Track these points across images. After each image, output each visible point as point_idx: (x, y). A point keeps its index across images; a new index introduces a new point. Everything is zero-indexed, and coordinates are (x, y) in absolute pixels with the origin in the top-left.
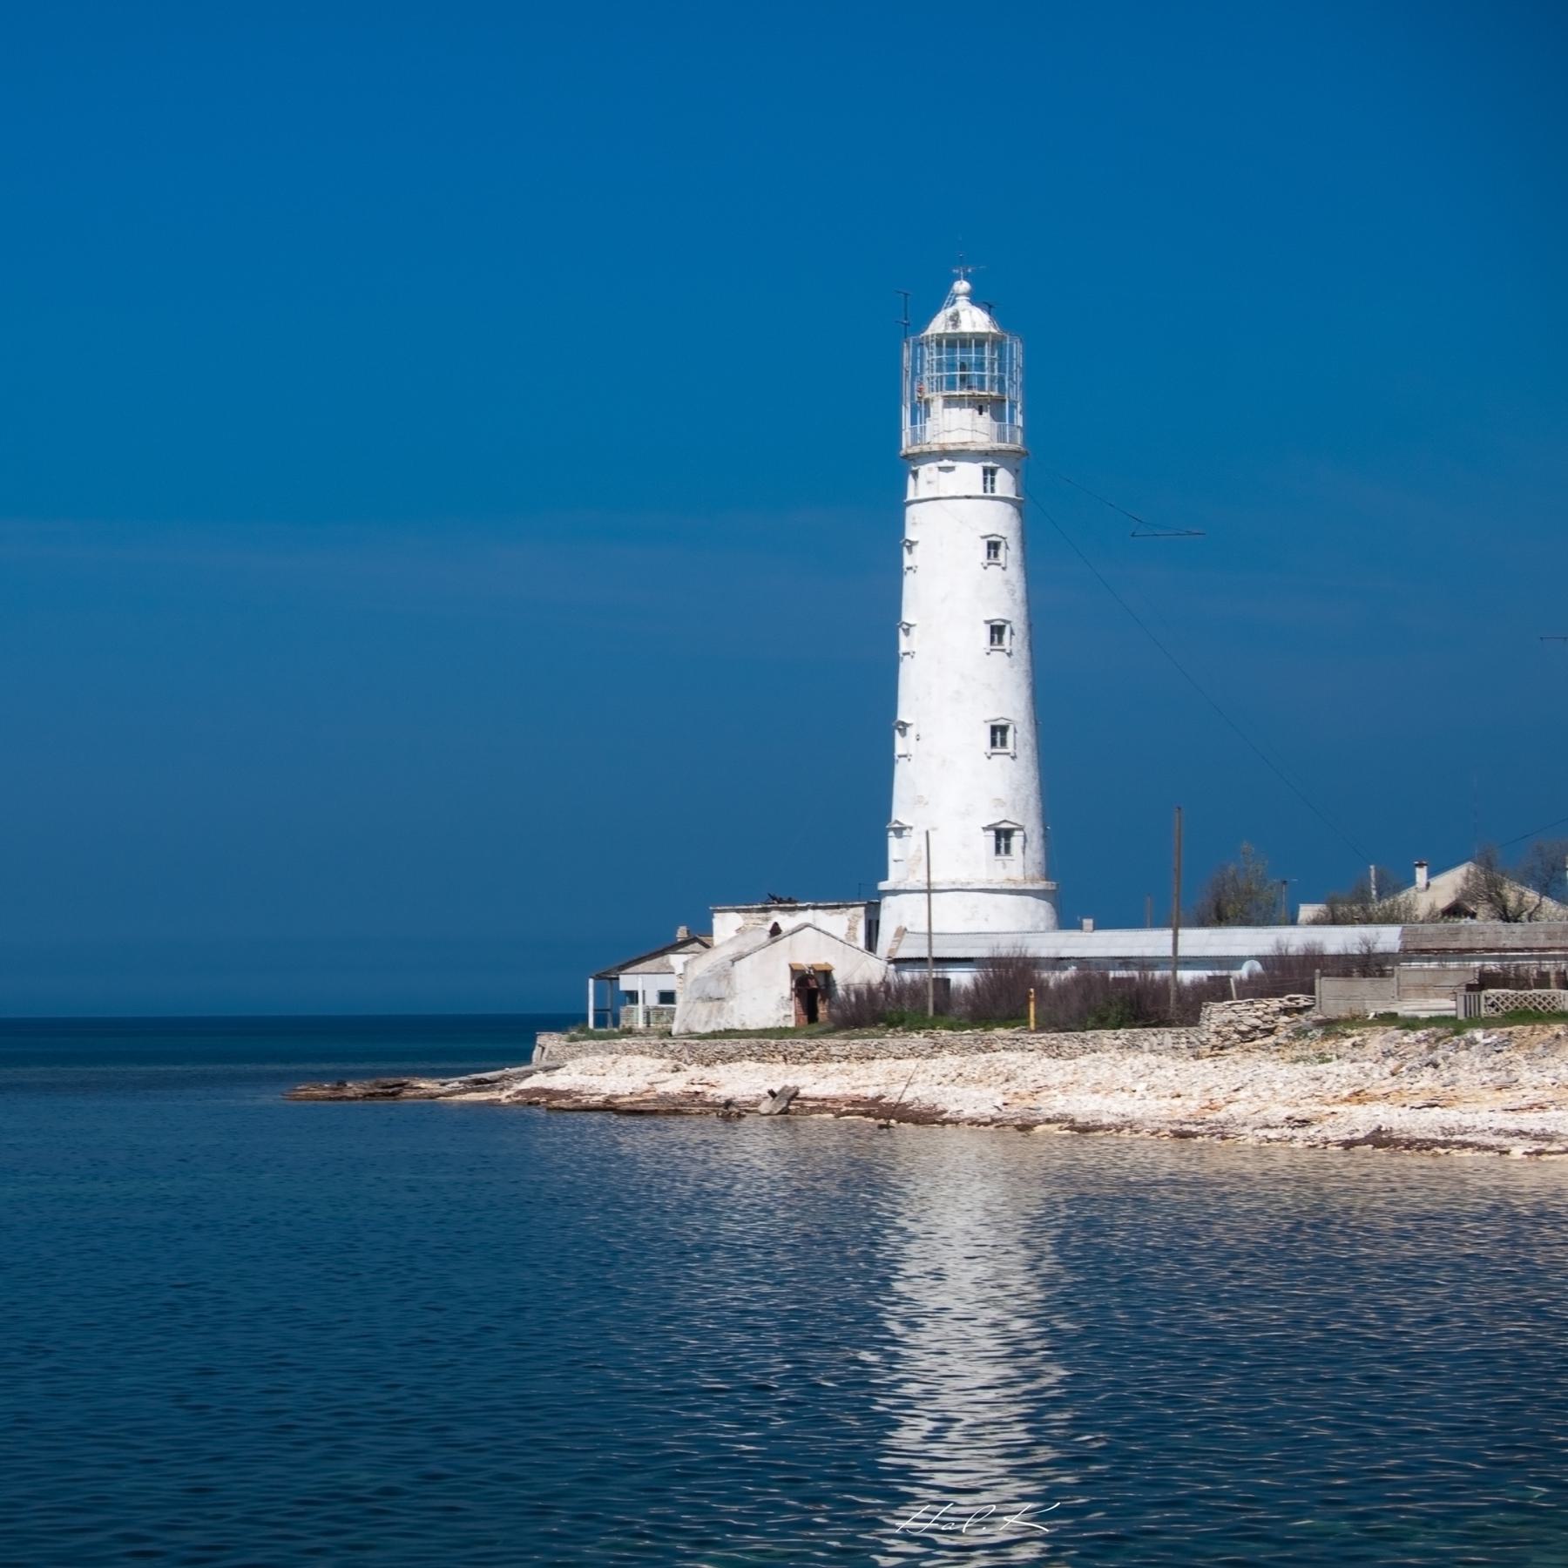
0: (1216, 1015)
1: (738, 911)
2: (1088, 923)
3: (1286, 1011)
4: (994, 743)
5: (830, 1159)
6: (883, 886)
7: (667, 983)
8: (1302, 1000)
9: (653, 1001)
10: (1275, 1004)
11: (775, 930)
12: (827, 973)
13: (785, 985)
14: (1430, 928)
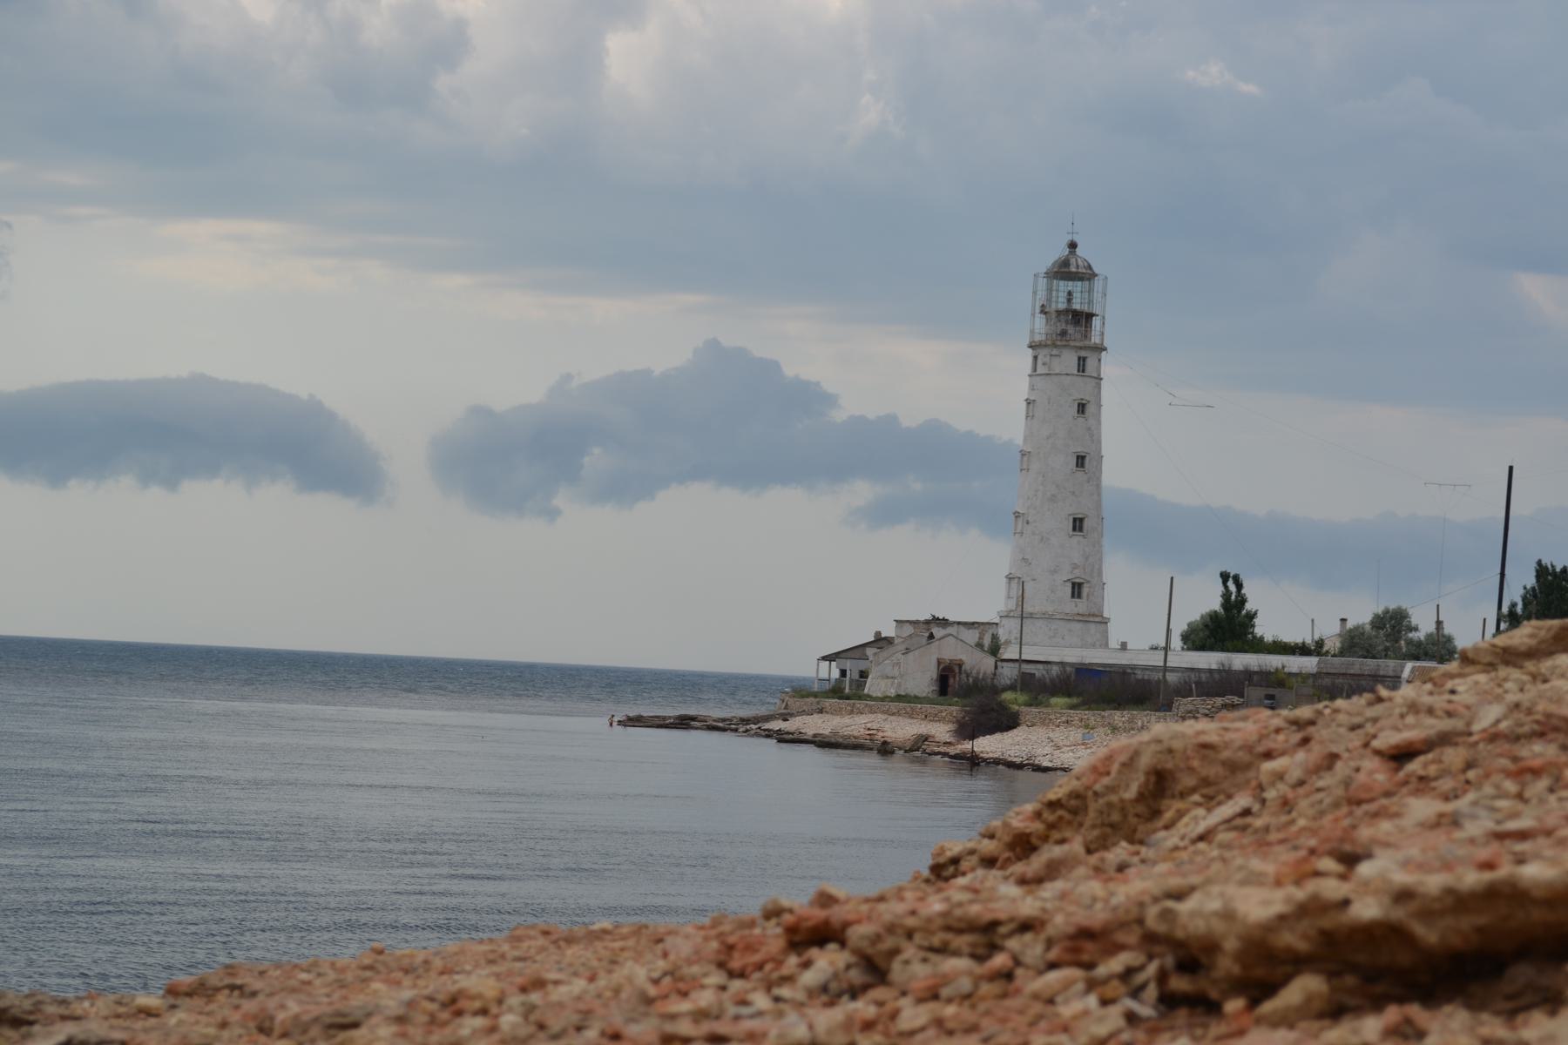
4: (1074, 529)
7: (862, 665)
8: (1236, 700)
11: (931, 636)
12: (960, 666)
13: (932, 673)
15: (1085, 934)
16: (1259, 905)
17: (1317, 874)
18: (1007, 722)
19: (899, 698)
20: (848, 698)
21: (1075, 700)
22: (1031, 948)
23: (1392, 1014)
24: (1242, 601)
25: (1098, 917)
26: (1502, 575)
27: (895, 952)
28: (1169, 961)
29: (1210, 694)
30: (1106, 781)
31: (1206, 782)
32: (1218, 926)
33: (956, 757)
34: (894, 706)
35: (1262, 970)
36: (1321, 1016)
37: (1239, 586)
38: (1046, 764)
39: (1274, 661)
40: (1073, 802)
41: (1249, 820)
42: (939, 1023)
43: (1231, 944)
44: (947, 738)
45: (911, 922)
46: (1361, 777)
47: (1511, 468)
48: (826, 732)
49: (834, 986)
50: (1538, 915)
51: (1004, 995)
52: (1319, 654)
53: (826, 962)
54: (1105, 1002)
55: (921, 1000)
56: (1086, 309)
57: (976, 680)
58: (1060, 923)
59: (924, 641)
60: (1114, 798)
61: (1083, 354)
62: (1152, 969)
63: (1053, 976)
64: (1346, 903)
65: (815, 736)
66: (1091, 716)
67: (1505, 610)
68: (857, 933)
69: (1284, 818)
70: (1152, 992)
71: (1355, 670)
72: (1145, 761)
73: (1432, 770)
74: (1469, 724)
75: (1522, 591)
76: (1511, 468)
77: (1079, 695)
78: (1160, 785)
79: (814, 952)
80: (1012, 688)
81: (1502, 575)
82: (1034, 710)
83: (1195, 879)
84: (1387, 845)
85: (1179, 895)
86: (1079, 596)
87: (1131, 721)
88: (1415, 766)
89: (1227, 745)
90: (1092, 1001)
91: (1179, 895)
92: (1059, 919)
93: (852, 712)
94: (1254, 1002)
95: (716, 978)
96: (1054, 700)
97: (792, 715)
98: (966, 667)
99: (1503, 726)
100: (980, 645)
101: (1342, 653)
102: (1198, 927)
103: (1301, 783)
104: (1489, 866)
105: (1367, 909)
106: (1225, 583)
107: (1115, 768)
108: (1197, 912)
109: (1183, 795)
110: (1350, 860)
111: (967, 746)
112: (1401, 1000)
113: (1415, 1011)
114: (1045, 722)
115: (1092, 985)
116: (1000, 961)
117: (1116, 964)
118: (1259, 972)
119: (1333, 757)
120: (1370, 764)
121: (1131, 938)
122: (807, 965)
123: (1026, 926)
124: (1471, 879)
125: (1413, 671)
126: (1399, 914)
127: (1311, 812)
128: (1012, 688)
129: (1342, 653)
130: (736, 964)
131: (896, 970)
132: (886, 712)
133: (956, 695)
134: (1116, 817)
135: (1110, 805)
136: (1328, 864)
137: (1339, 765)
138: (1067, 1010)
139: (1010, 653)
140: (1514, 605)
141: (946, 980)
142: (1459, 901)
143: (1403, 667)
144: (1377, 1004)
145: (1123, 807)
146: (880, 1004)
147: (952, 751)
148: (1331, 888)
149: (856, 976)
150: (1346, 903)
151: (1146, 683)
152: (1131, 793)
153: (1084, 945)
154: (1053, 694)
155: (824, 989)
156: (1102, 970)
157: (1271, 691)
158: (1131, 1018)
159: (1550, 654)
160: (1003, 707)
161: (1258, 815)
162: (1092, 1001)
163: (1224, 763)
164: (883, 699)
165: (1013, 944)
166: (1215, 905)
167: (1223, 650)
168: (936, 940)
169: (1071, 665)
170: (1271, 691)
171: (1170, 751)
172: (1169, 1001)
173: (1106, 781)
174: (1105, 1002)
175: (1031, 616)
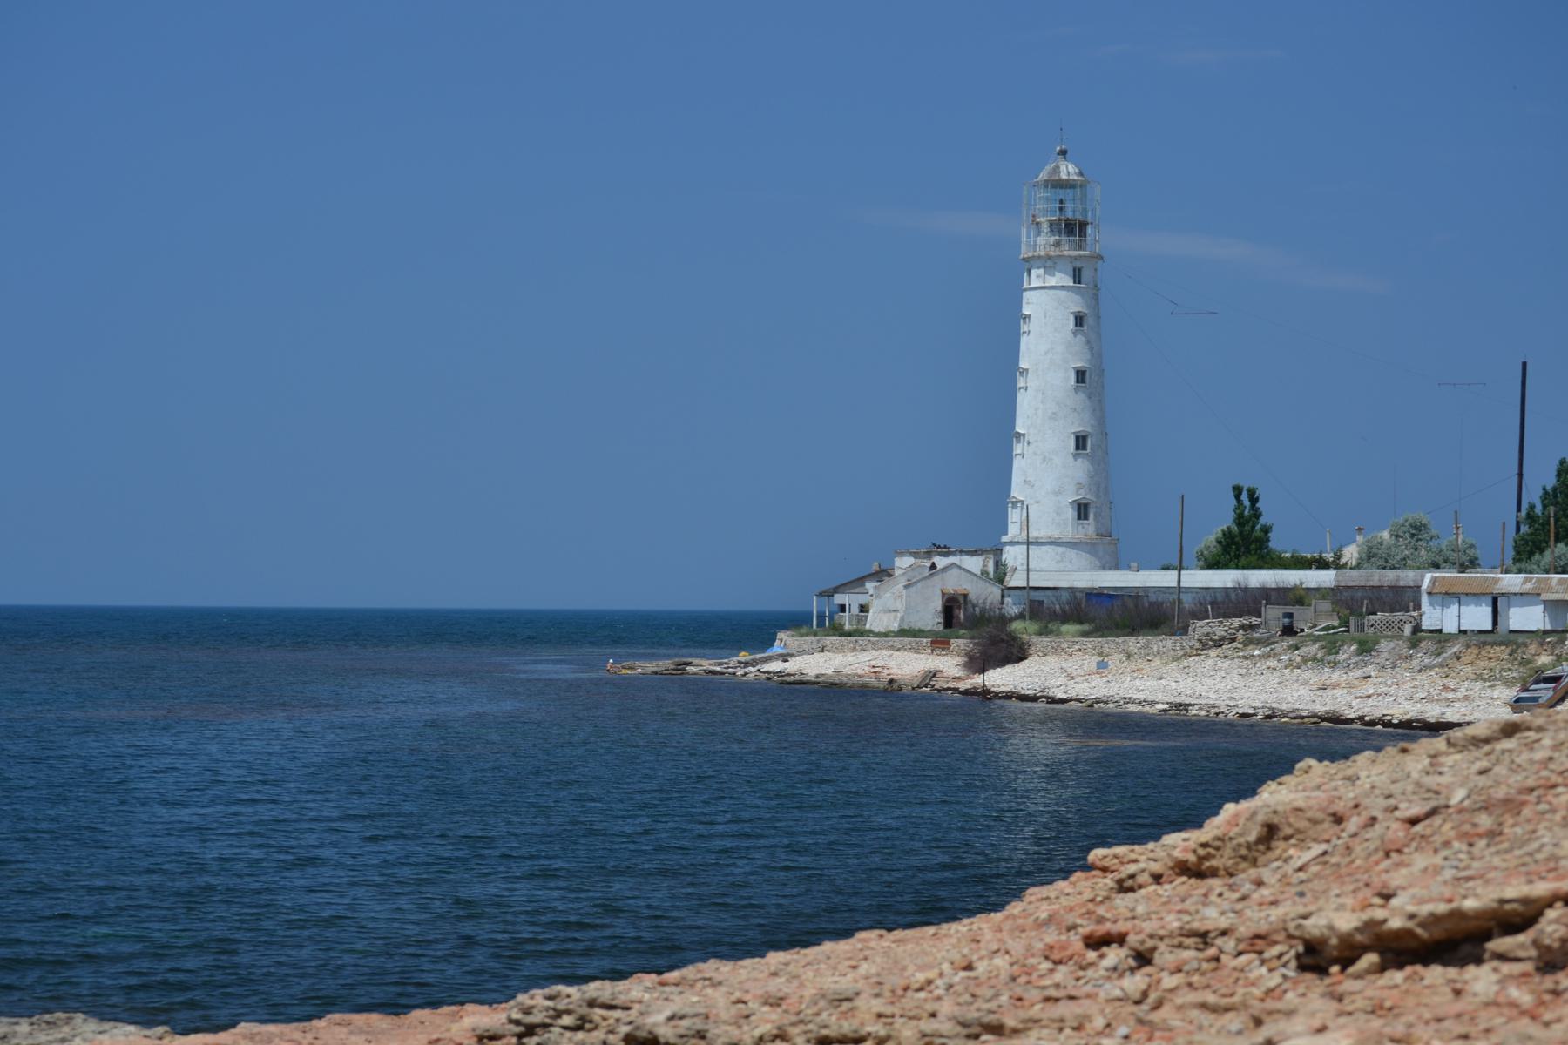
0: (1200, 628)
1: (481, 1003)
2: (1134, 565)
3: (1242, 627)
4: (1077, 448)
5: (1040, 731)
6: (1005, 539)
7: (863, 599)
8: (1254, 620)
9: (855, 610)
10: (1237, 622)
11: (933, 566)
12: (965, 596)
13: (938, 604)
14: (1355, 572)
15: (1258, 937)
16: (1346, 922)
17: (1371, 905)
18: (1014, 653)
19: (902, 633)
20: (849, 635)
21: (1086, 627)
22: (1229, 944)
23: (1409, 970)
24: (1257, 514)
25: (1263, 928)
26: (1520, 475)
27: (1154, 949)
28: (1301, 949)
29: (1226, 616)
30: (1236, 830)
31: (1299, 831)
32: (1326, 932)
33: (966, 692)
34: (898, 641)
35: (1348, 953)
36: (1375, 972)
37: (1254, 500)
38: (1060, 695)
39: (1291, 577)
40: (1218, 843)
41: (1327, 858)
42: (1190, 985)
43: (1334, 941)
44: (957, 672)
45: (1162, 932)
46: (1390, 834)
47: (1524, 365)
48: (829, 672)
49: (1121, 967)
50: (1473, 924)
51: (1215, 970)
52: (1338, 567)
53: (1114, 955)
54: (1271, 970)
55: (1172, 973)
56: (1079, 217)
57: (983, 610)
58: (1244, 930)
59: (927, 573)
60: (1242, 840)
61: (1078, 264)
62: (1293, 952)
63: (1243, 958)
64: (1385, 921)
65: (817, 677)
66: (1106, 643)
67: (1523, 513)
68: (1132, 939)
69: (1348, 859)
70: (1293, 964)
71: (1375, 582)
72: (1260, 818)
73: (1428, 831)
74: (1448, 799)
75: (1541, 492)
76: (1524, 365)
77: (1089, 621)
78: (1270, 832)
79: (1105, 949)
80: (1021, 616)
81: (1520, 475)
82: (1045, 640)
83: (1312, 908)
84: (1404, 888)
85: (1305, 917)
86: (1086, 518)
87: (1146, 646)
88: (1418, 828)
89: (1310, 808)
90: (1264, 970)
91: (1305, 917)
92: (1242, 929)
93: (854, 649)
94: (1343, 970)
95: (1046, 965)
96: (1065, 628)
97: (792, 655)
98: (972, 597)
99: (1466, 803)
100: (984, 572)
101: (1358, 566)
102: (1316, 932)
103: (1355, 835)
104: (1450, 901)
105: (1396, 923)
106: (1238, 497)
107: (1242, 821)
108: (1315, 926)
109: (1286, 838)
110: (1387, 897)
111: (977, 680)
112: (1412, 963)
113: (1418, 968)
114: (1056, 650)
115: (1263, 962)
116: (1212, 951)
117: (1276, 950)
118: (1347, 954)
119: (1374, 819)
120: (1395, 825)
121: (1281, 937)
122: (1102, 956)
123: (1224, 933)
124: (1442, 908)
125: (1434, 580)
126: (1410, 924)
127: (1363, 854)
128: (1021, 616)
129: (1358, 566)
130: (1056, 957)
131: (1157, 958)
132: (892, 647)
133: (962, 626)
134: (1244, 852)
135: (1240, 845)
136: (1377, 900)
137: (1377, 826)
138: (1253, 976)
139: (1016, 580)
140: (1532, 507)
141: (1185, 962)
142: (1435, 919)
143: (1423, 577)
144: (1400, 967)
145: (1249, 846)
146: (1150, 975)
147: (963, 686)
148: (1379, 914)
149: (1132, 962)
150: (1385, 921)
151: (1157, 605)
152: (1252, 837)
153: (1258, 941)
154: (1064, 622)
155: (1115, 969)
156: (1266, 955)
157: (1289, 609)
158: (1285, 977)
159: (1498, 739)
160: (1013, 638)
161: (1332, 855)
162: (1264, 970)
163: (1310, 820)
164: (886, 635)
165: (1219, 942)
166: (1323, 922)
167: (1237, 567)
168: (1176, 942)
169: (1082, 590)
170: (1289, 609)
171: (1275, 812)
172: (1302, 968)
173: (1236, 830)
174: (1271, 970)
175: (1038, 543)
